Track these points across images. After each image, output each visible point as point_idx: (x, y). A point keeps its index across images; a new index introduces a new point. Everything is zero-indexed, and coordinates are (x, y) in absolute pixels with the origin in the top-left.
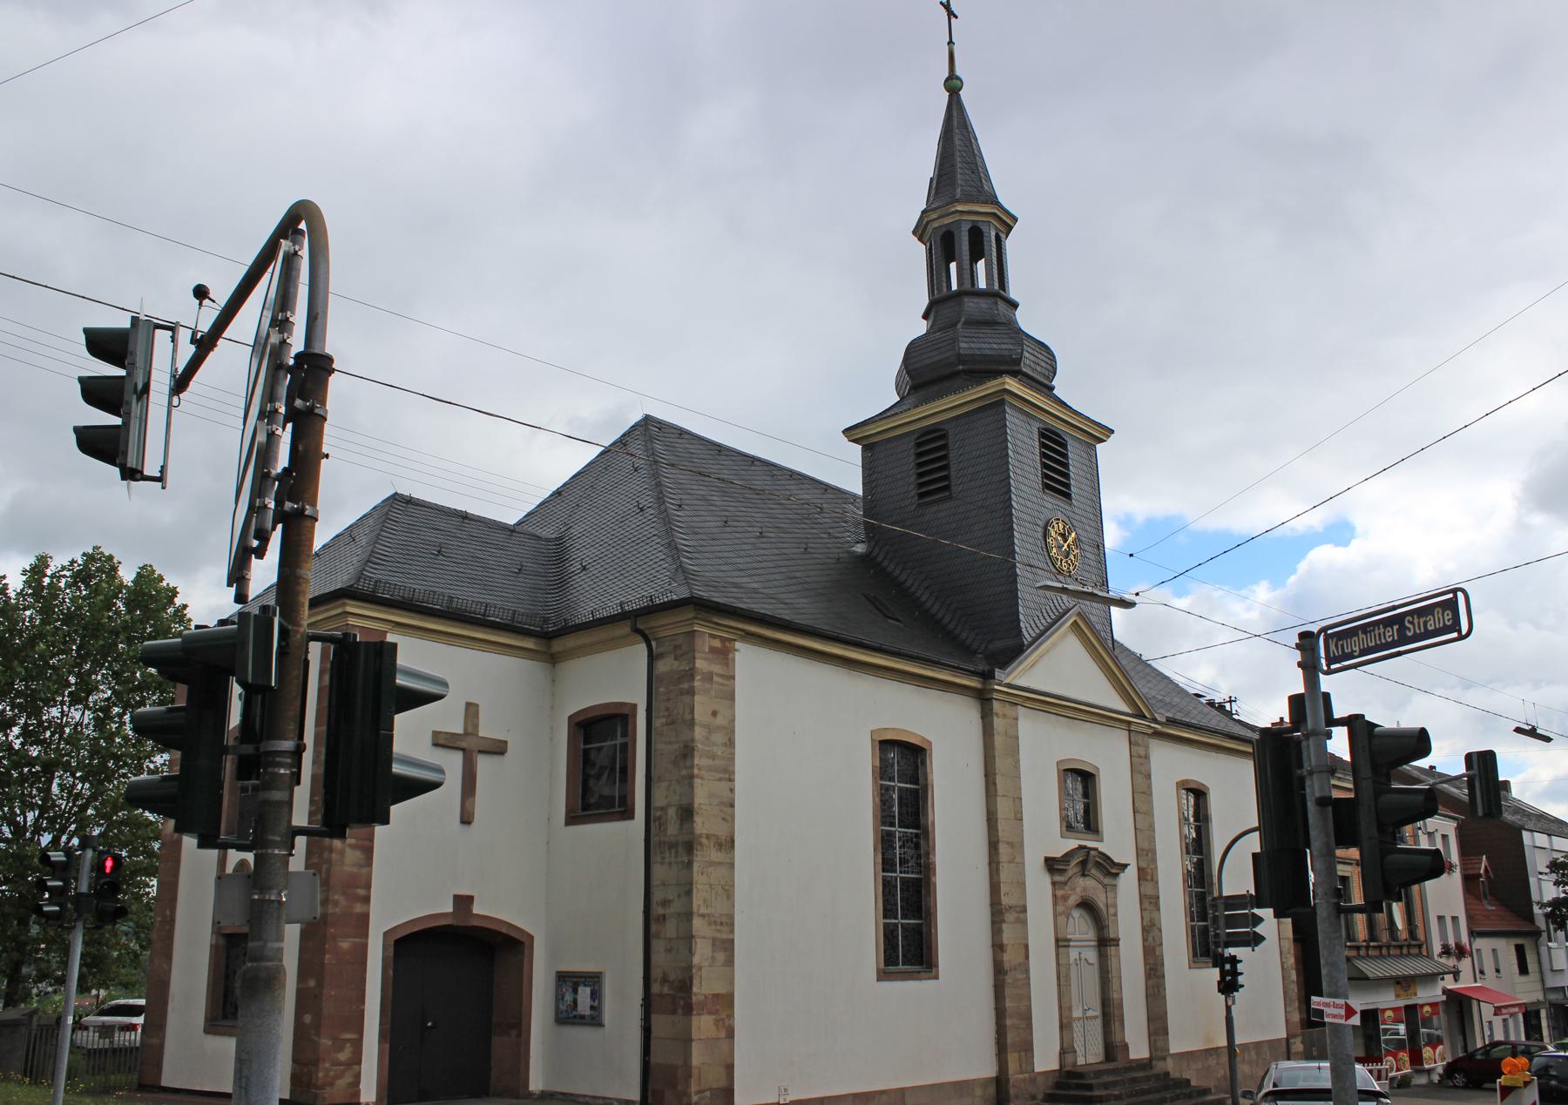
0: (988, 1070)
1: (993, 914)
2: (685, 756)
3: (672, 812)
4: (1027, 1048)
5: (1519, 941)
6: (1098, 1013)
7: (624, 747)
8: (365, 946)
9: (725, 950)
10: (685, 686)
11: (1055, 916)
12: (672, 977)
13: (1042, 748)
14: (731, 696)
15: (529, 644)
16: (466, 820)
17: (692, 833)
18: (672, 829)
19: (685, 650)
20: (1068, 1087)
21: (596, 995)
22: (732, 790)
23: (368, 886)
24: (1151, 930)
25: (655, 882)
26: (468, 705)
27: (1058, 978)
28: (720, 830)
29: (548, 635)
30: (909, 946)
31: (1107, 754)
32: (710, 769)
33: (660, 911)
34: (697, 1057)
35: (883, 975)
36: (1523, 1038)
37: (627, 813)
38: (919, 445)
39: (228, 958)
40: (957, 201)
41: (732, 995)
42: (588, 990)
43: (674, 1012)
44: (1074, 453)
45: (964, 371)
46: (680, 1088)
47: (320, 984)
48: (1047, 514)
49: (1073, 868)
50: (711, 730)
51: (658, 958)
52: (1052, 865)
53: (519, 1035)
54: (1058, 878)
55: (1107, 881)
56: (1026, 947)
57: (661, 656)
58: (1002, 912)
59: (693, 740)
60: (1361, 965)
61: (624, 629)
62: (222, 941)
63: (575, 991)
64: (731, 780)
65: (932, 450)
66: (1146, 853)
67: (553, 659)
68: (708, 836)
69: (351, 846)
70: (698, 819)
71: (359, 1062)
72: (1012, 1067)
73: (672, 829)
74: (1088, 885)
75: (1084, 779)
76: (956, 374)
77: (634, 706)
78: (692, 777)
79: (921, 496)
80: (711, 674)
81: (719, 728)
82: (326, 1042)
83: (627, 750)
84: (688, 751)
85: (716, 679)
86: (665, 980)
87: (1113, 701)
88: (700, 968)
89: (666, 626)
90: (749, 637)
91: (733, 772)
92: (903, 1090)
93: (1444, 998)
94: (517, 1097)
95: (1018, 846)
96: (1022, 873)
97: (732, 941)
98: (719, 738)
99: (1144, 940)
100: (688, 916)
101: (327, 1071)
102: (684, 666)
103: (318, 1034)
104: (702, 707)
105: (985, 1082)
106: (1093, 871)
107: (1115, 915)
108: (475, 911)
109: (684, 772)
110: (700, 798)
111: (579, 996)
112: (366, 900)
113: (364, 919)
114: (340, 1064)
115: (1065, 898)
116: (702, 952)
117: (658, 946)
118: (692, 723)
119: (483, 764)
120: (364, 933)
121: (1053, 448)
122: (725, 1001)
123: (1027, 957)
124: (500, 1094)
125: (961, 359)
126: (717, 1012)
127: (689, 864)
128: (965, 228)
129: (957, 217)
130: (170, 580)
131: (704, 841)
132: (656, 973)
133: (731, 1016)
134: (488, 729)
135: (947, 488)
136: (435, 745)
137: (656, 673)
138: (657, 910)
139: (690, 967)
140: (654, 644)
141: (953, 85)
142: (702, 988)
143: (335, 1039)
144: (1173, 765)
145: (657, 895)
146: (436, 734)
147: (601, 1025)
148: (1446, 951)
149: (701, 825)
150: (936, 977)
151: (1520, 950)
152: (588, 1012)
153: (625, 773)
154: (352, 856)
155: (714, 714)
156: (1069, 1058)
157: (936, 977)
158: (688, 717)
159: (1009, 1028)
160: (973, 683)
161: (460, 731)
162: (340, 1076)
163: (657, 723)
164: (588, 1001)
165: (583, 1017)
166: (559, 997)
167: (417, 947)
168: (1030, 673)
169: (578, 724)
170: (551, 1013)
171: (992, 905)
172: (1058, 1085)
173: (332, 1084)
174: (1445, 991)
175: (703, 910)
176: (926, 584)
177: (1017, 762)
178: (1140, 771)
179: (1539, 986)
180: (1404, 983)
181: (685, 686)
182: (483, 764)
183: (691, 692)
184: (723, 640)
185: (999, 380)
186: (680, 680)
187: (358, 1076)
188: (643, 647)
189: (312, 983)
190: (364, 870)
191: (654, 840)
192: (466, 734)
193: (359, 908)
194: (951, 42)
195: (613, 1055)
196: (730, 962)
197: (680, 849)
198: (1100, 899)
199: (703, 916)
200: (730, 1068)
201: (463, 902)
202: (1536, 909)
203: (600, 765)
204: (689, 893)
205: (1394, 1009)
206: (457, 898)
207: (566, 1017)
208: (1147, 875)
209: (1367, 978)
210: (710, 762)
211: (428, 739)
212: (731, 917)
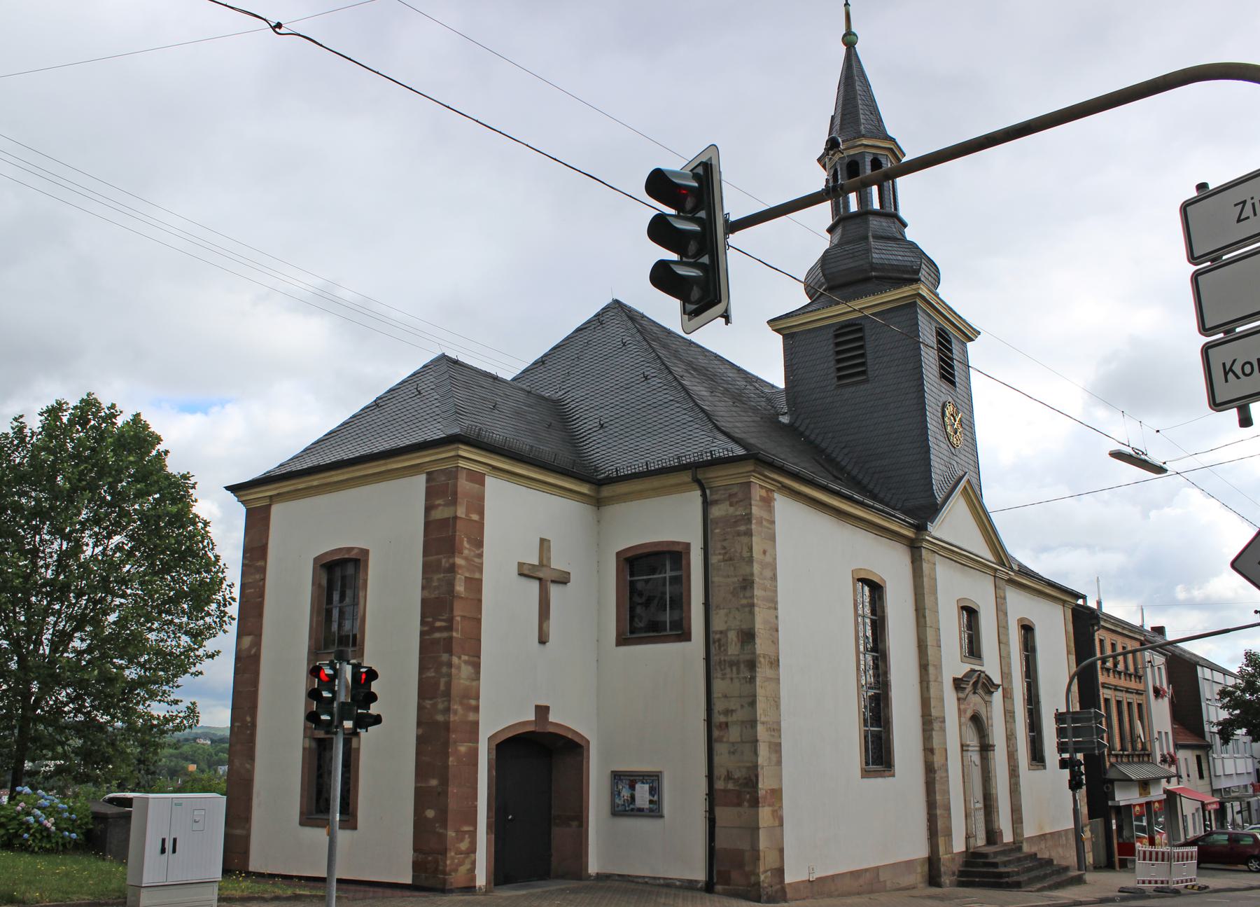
0: (922, 852)
1: (924, 724)
2: (744, 588)
3: (732, 635)
4: (949, 834)
5: (1198, 752)
6: (980, 805)
7: (677, 580)
8: (477, 749)
10: (743, 528)
12: (737, 775)
13: (953, 586)
14: (773, 538)
15: (584, 489)
16: (543, 641)
17: (754, 653)
18: (733, 649)
19: (742, 496)
20: (977, 865)
21: (655, 790)
23: (478, 698)
24: (1010, 737)
25: (716, 694)
26: (542, 541)
29: (599, 486)
31: (981, 592)
33: (722, 719)
34: (763, 843)
37: (685, 636)
38: (837, 336)
39: (319, 759)
40: (863, 136)
41: (781, 790)
42: (647, 787)
43: (739, 805)
44: (956, 347)
45: (876, 277)
46: (747, 869)
47: (444, 781)
48: (943, 399)
51: (722, 758)
52: (958, 684)
53: (581, 825)
54: (961, 695)
55: (987, 698)
57: (716, 502)
58: (929, 722)
59: (752, 575)
60: (1121, 768)
61: (686, 477)
62: (314, 745)
63: (632, 787)
64: (776, 609)
65: (849, 338)
66: (1006, 675)
67: (598, 503)
69: (466, 662)
70: (758, 641)
72: (942, 849)
73: (733, 649)
74: (975, 701)
75: (971, 613)
76: (868, 279)
77: (688, 545)
78: (752, 605)
79: (840, 378)
82: (451, 834)
83: (682, 581)
85: (765, 523)
86: (729, 777)
87: (986, 553)
89: (721, 478)
92: (877, 868)
93: (1165, 796)
94: (580, 879)
95: (939, 667)
96: (942, 691)
98: (768, 573)
100: (753, 723)
101: (453, 858)
102: (740, 511)
103: (445, 827)
104: (757, 544)
106: (980, 691)
108: (551, 720)
109: (744, 601)
110: (759, 626)
111: (637, 794)
112: (476, 709)
117: (720, 748)
118: (750, 560)
119: (554, 590)
120: (474, 737)
121: (944, 340)
122: (777, 794)
124: (563, 876)
125: (873, 267)
127: (752, 680)
128: (868, 159)
129: (861, 150)
130: (155, 428)
132: (719, 771)
135: (863, 373)
136: (521, 574)
137: (711, 516)
138: (719, 718)
139: (756, 767)
140: (708, 492)
141: (849, 40)
142: (764, 785)
143: (457, 831)
144: (1021, 605)
145: (719, 706)
146: (521, 565)
147: (662, 816)
148: (1164, 760)
149: (761, 646)
151: (1198, 758)
152: (647, 805)
153: (680, 602)
154: (466, 670)
155: (765, 552)
156: (972, 841)
158: (746, 554)
160: (909, 533)
161: (536, 563)
162: (461, 863)
163: (714, 560)
164: (647, 797)
165: (641, 810)
166: (615, 793)
169: (323, 566)
170: (606, 808)
171: (923, 716)
172: (967, 864)
173: (456, 870)
174: (1166, 791)
175: (763, 719)
176: (846, 451)
177: (936, 599)
178: (1001, 610)
179: (1208, 788)
180: (1145, 785)
181: (743, 528)
182: (554, 590)
183: (749, 533)
184: (769, 490)
185: (914, 286)
186: (736, 523)
187: (474, 863)
188: (699, 493)
190: (474, 683)
191: (714, 659)
192: (541, 565)
193: (471, 717)
195: (674, 844)
197: (738, 663)
202: (1206, 728)
203: (649, 597)
204: (753, 704)
205: (1141, 805)
206: (537, 707)
207: (622, 809)
208: (1007, 695)
209: (1131, 780)
211: (514, 570)
212: (779, 723)
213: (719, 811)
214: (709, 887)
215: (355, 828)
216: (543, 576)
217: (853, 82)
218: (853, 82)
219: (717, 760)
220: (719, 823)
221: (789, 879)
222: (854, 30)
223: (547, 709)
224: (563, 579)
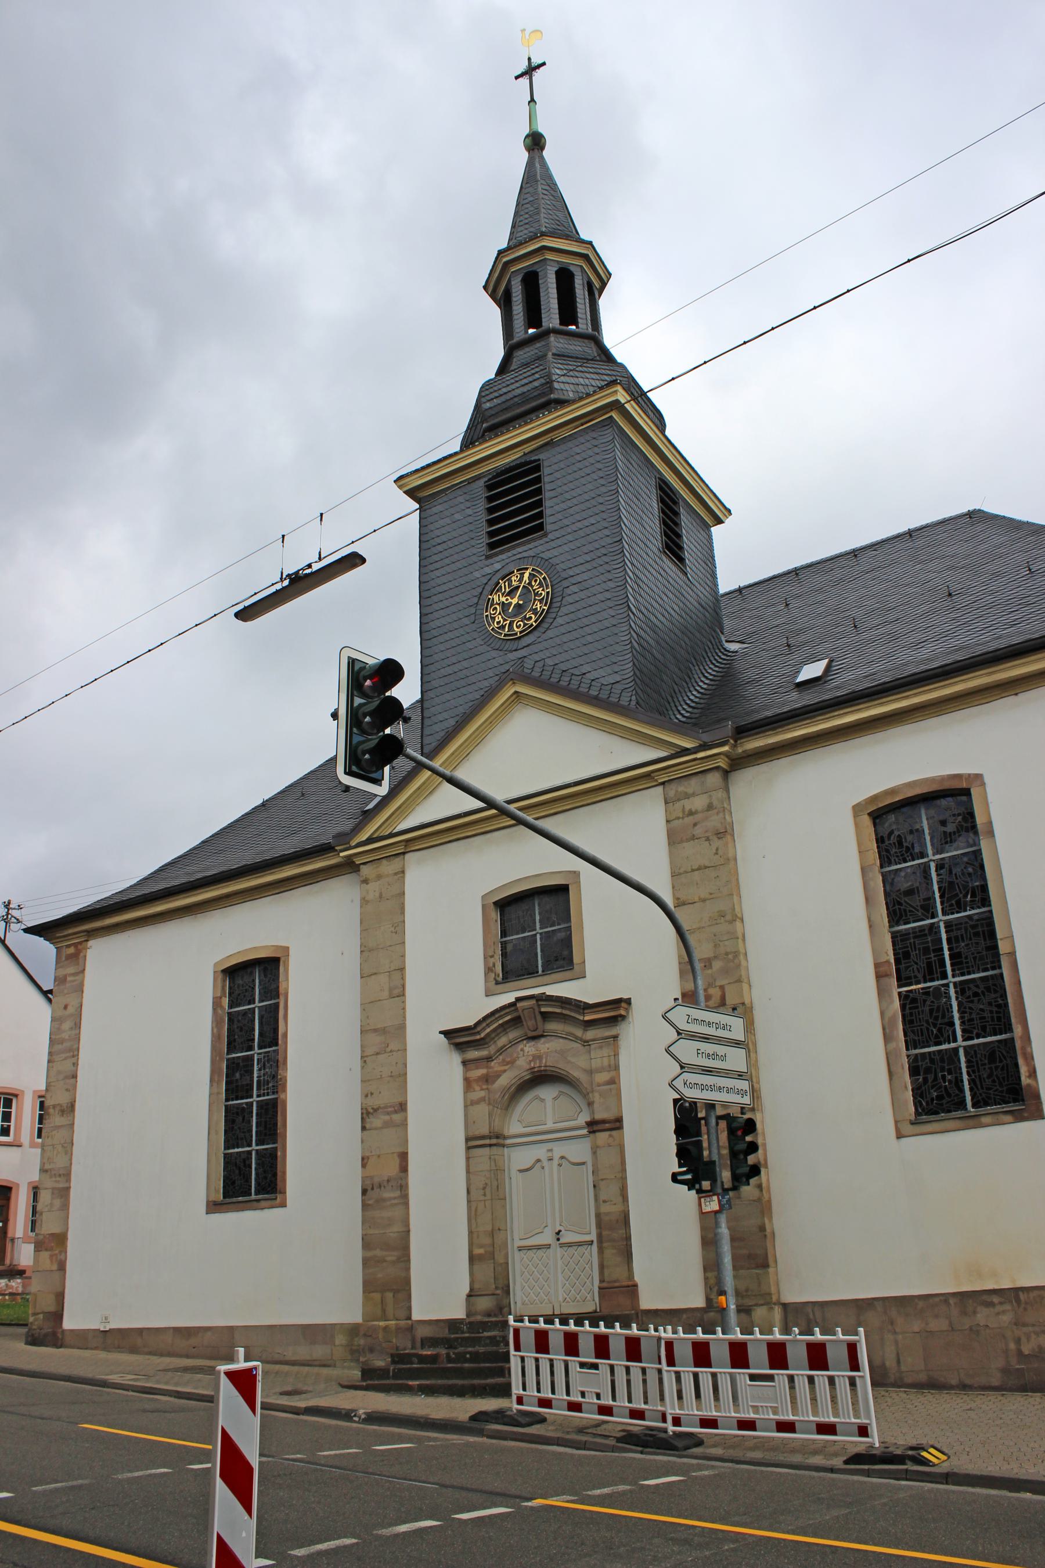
9: (62, 1197)
30: (250, 1170)
36: (590, 330)
54: (473, 1054)
56: (404, 1156)
58: (383, 1112)
68: (54, 1107)
80: (65, 977)
85: (69, 979)
90: (92, 934)
92: (231, 1329)
107: (614, 1081)
115: (487, 1079)
123: (404, 1169)
126: (51, 1249)
141: (535, 142)
150: (283, 1205)
155: (66, 1007)
157: (283, 1205)
159: (386, 1266)
184: (75, 945)
194: (532, 100)
221: (68, 1324)
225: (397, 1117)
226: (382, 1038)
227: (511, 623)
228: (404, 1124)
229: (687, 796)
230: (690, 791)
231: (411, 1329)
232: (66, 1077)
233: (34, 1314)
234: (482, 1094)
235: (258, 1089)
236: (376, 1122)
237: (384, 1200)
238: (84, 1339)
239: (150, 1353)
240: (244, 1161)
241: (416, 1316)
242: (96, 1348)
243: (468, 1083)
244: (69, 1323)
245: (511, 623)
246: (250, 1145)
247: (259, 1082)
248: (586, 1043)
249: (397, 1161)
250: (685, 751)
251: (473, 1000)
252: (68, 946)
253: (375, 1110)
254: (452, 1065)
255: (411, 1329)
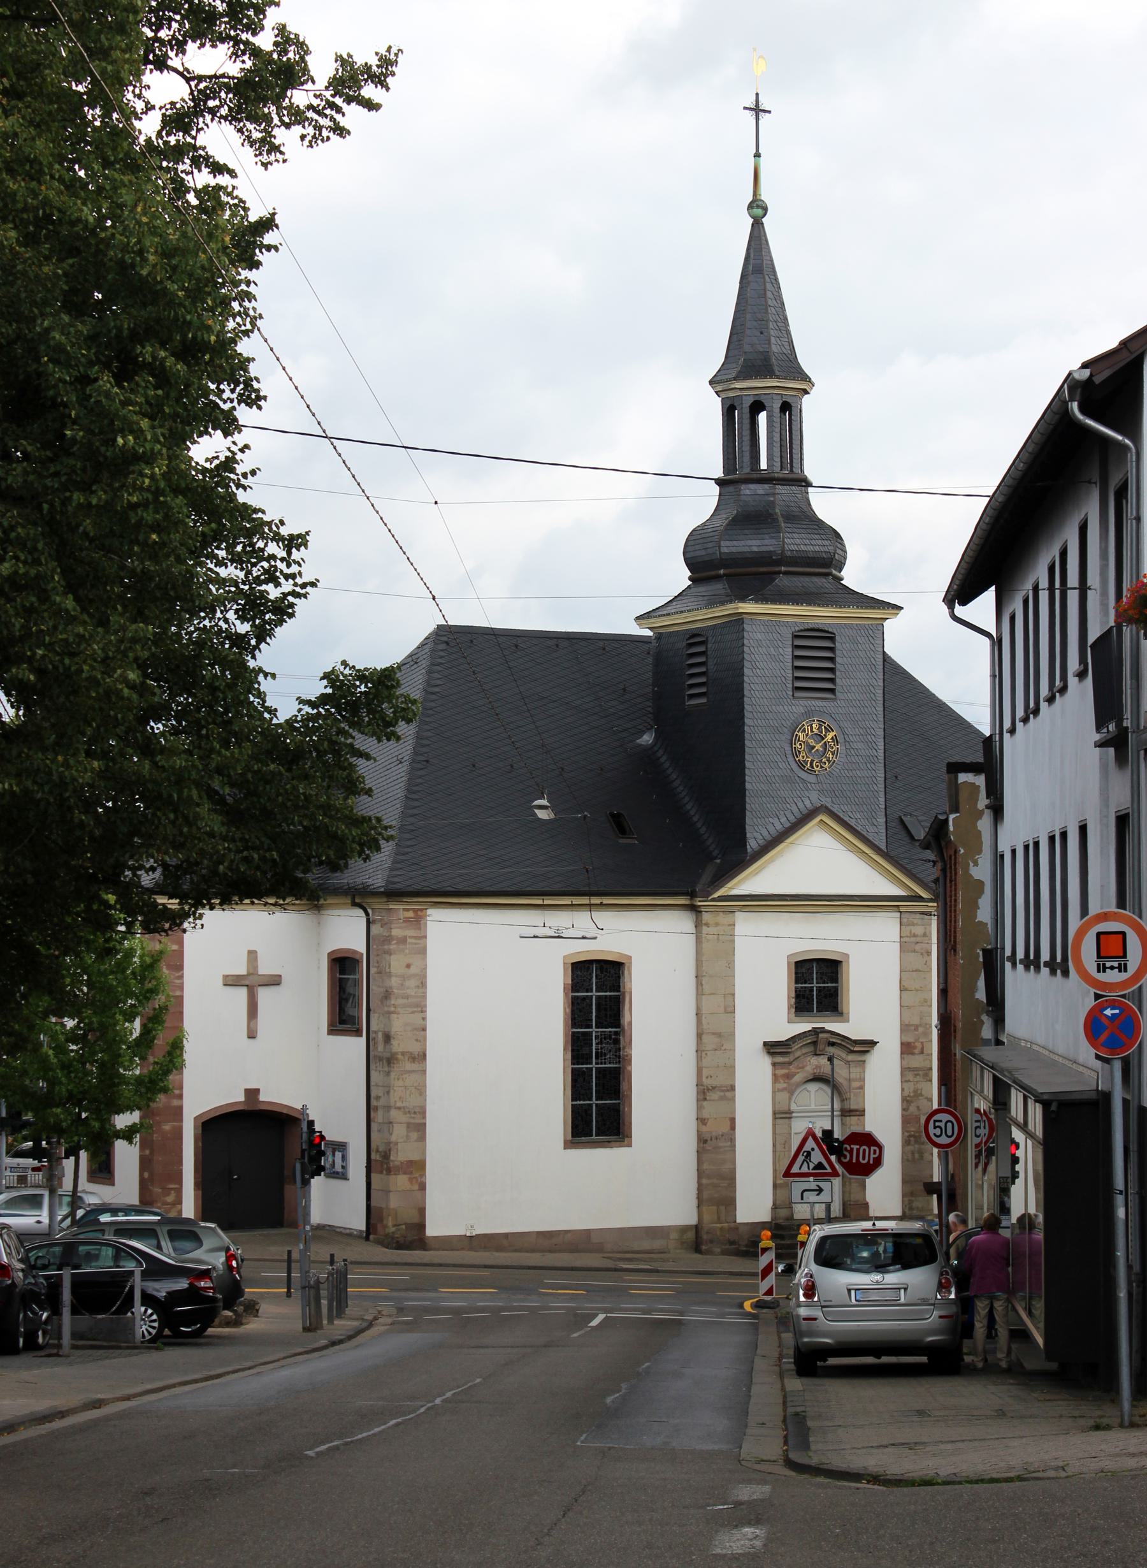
3: (380, 1035)
11: (774, 1092)
14: (423, 951)
16: (252, 1035)
18: (380, 1048)
21: (344, 1158)
22: (424, 1019)
23: (181, 1088)
27: (774, 1145)
28: (414, 1048)
32: (404, 1006)
35: (568, 1145)
37: (361, 1036)
43: (381, 1172)
49: (797, 1050)
50: (404, 977)
54: (779, 1059)
56: (733, 1120)
57: (374, 921)
58: (713, 1090)
63: (334, 1155)
64: (423, 1011)
68: (403, 1054)
71: (181, 1203)
73: (380, 1048)
80: (405, 938)
81: (414, 975)
84: (387, 995)
85: (409, 940)
86: (377, 1151)
88: (397, 1144)
91: (425, 1006)
97: (425, 1124)
98: (412, 983)
99: (903, 1110)
105: (684, 1229)
107: (862, 1088)
113: (180, 1110)
114: (168, 1204)
115: (788, 1077)
116: (399, 1132)
117: (374, 1126)
119: (263, 994)
123: (733, 1128)
126: (411, 1173)
131: (400, 1056)
133: (423, 1175)
134: (265, 969)
138: (374, 1103)
140: (370, 911)
141: (757, 208)
142: (401, 1155)
143: (164, 1188)
145: (373, 1094)
146: (226, 977)
149: (397, 1046)
150: (630, 1145)
155: (408, 966)
157: (630, 1145)
161: (244, 972)
163: (373, 970)
165: (338, 1173)
167: (219, 1127)
168: (761, 878)
175: (399, 1104)
182: (263, 994)
189: (147, 1152)
191: (372, 1054)
196: (422, 1138)
198: (841, 1073)
199: (399, 1108)
200: (422, 1211)
201: (251, 1094)
203: (349, 997)
210: (405, 1001)
213: (373, 1175)
214: (367, 1239)
215: (113, 1185)
216: (252, 983)
217: (758, 269)
218: (758, 269)
219: (373, 1135)
220: (373, 1186)
222: (764, 196)
223: (257, 1091)
224: (275, 981)
225: (728, 1094)
226: (712, 1037)
227: (812, 761)
228: (733, 1099)
229: (913, 924)
230: (915, 921)
231: (737, 1229)
232: (416, 1029)
233: (394, 1226)
234: (785, 1085)
235: (597, 1058)
236: (713, 1096)
237: (720, 1147)
238: (447, 1243)
239: (515, 1251)
240: (586, 1111)
241: (738, 1221)
242: (462, 1249)
243: (776, 1079)
244: (430, 1231)
245: (812, 761)
246: (591, 1099)
247: (597, 1053)
248: (848, 1062)
249: (729, 1123)
250: (919, 898)
251: (786, 1026)
252: (408, 910)
253: (714, 1088)
254: (765, 1064)
255: (737, 1229)
